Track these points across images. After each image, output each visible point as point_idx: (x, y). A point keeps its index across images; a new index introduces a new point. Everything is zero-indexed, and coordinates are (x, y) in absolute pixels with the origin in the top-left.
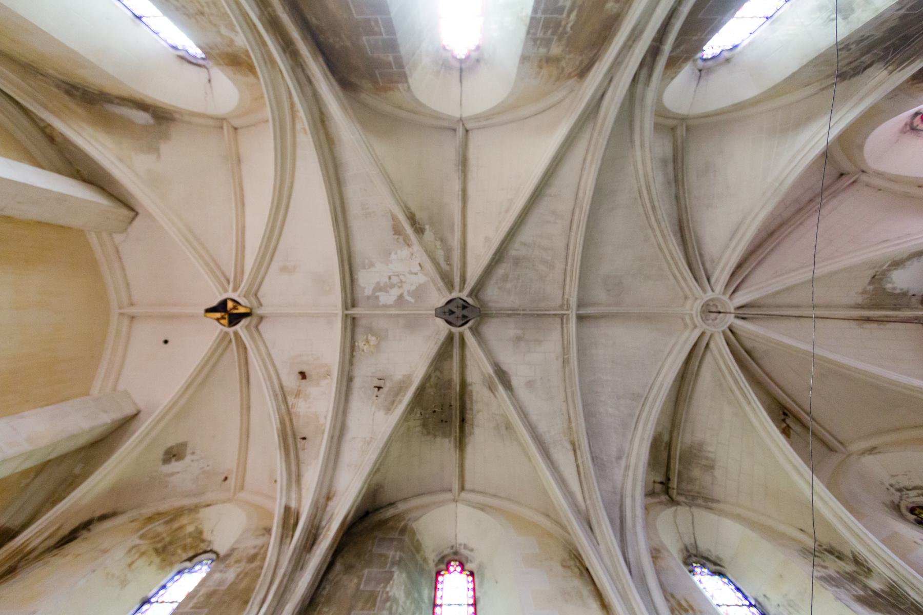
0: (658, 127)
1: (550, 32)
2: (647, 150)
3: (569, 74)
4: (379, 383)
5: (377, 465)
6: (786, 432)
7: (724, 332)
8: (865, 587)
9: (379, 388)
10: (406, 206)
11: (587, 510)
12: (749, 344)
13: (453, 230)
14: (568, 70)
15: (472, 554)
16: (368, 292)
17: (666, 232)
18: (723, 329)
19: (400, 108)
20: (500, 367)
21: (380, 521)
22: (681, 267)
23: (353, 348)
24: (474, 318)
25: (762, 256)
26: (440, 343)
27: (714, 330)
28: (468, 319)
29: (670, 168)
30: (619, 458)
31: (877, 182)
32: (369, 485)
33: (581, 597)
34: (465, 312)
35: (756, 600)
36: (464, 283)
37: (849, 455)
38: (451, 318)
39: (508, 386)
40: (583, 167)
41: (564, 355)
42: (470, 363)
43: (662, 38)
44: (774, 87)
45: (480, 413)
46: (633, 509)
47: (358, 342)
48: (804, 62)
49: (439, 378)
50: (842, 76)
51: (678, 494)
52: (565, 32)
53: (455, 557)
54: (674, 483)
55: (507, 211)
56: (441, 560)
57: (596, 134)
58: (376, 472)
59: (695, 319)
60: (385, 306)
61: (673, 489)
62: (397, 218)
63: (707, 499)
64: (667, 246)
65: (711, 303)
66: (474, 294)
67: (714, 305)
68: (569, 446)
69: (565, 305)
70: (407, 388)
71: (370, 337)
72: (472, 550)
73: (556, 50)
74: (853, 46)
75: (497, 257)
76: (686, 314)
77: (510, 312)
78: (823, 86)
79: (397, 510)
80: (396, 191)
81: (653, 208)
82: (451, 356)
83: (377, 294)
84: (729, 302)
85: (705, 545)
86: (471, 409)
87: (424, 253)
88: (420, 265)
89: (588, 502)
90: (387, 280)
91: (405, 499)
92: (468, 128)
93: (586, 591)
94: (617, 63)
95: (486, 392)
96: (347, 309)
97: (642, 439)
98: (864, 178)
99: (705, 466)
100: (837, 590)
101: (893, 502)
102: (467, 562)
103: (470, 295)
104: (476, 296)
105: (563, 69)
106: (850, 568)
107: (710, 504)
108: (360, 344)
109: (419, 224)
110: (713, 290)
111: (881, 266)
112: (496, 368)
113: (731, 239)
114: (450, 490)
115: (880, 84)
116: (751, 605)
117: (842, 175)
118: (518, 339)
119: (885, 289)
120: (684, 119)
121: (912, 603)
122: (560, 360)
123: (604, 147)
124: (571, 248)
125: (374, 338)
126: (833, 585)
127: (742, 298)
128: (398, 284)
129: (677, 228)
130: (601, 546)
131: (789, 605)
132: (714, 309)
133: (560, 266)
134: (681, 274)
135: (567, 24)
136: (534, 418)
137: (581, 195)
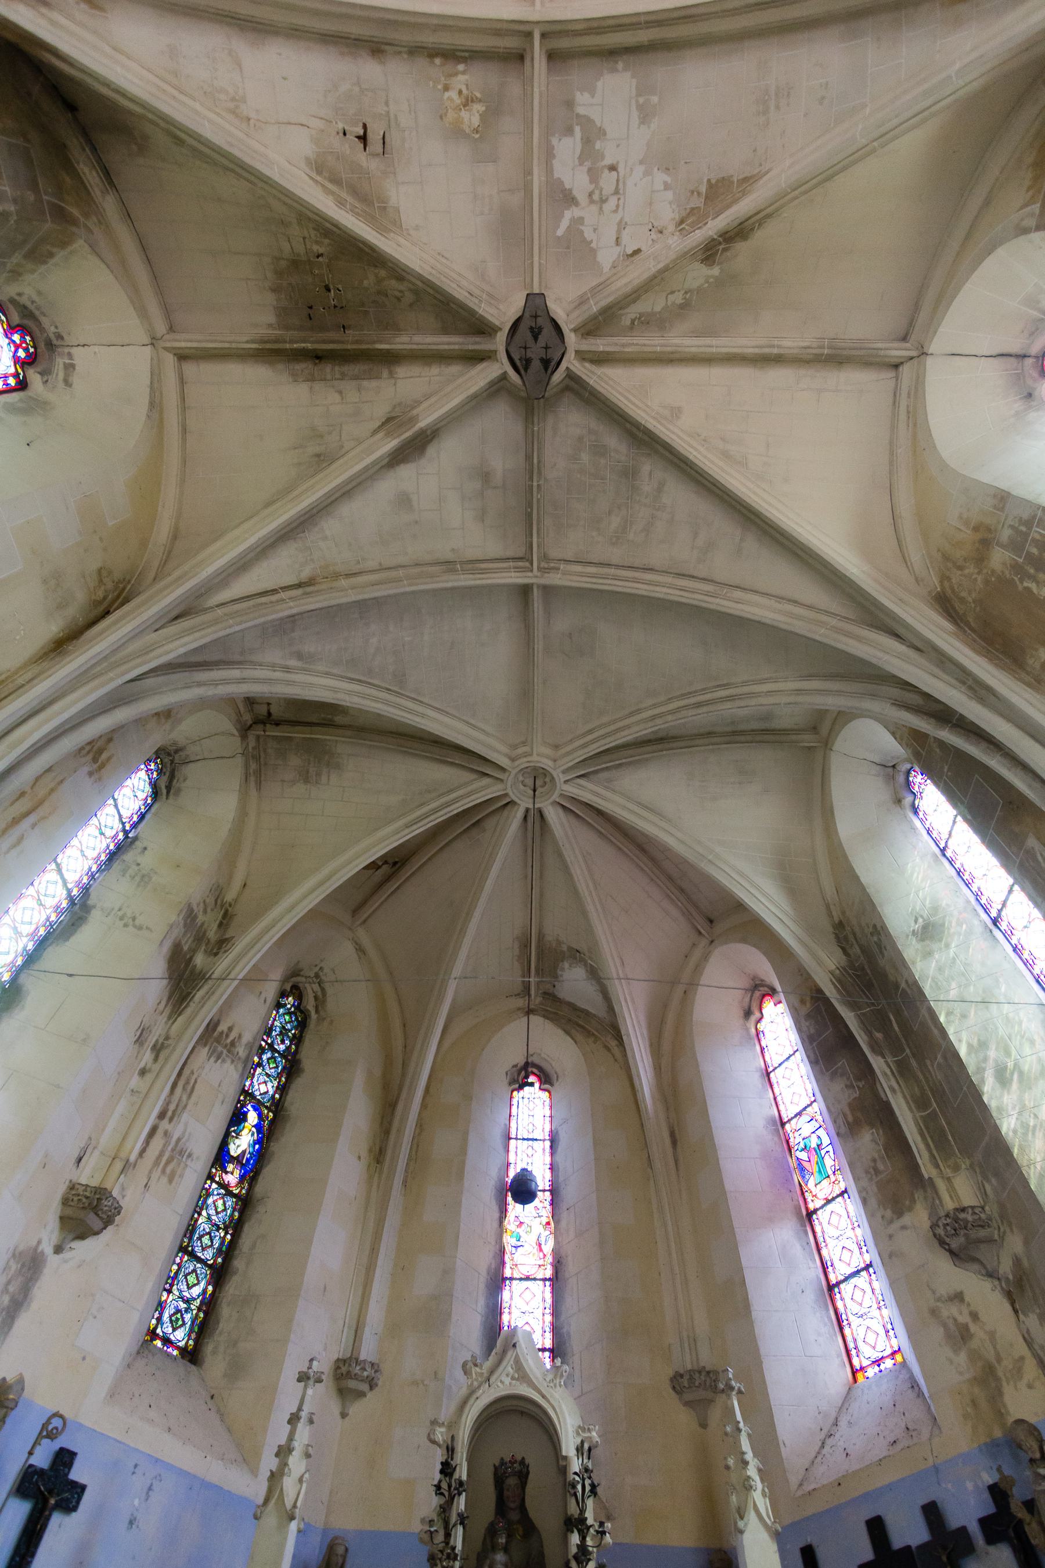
0: (821, 714)
1: (1035, 551)
2: (792, 699)
3: (949, 579)
4: (374, 137)
5: (190, 141)
6: (373, 866)
7: (506, 795)
8: (194, 951)
9: (363, 139)
10: (769, 216)
11: (206, 610)
12: (490, 824)
13: (697, 334)
14: (956, 577)
15: (61, 384)
16: (585, 104)
17: (658, 721)
18: (511, 794)
19: (987, 202)
20: (431, 440)
21: (65, 146)
22: (603, 742)
23: (451, 55)
24: (524, 384)
25: (612, 839)
26: (472, 303)
27: (509, 783)
28: (522, 372)
29: (755, 725)
30: (300, 656)
31: (697, 954)
32: (141, 117)
33: (60, 606)
34: (536, 364)
35: (136, 839)
36: (592, 362)
37: (350, 929)
38: (523, 329)
39: (399, 457)
40: (783, 598)
41: (462, 563)
42: (435, 372)
43: (962, 728)
44: (845, 857)
45: (337, 396)
46: (226, 682)
47: (464, 73)
48: (871, 891)
49: (399, 299)
50: (839, 927)
51: (258, 737)
52: (1025, 576)
53: (42, 346)
54: (273, 732)
55: (726, 455)
56: (26, 312)
57: (834, 622)
58: (176, 137)
59: (525, 760)
60: (549, 154)
61: (264, 731)
62: (744, 193)
63: (258, 774)
64: (638, 723)
65: (547, 780)
66: (572, 384)
67: (545, 783)
68: (305, 575)
69: (549, 564)
70: (371, 219)
71: (479, 107)
72: (67, 383)
73: (999, 558)
74: (875, 939)
75: (640, 435)
76: (532, 749)
77: (535, 461)
78: (832, 907)
79: (98, 193)
80: (806, 192)
81: (699, 705)
82: (445, 331)
83: (577, 129)
84: (551, 800)
85: (192, 775)
86: (343, 377)
87: (661, 266)
88: (637, 252)
89: (220, 612)
90: (608, 161)
91: (128, 215)
92: (901, 369)
93: (74, 611)
94: (942, 660)
95: (381, 410)
96: (543, 35)
97: (335, 690)
98: (704, 942)
99: (308, 772)
100: (182, 925)
101: (301, 970)
102: (41, 374)
103: (570, 375)
104: (567, 388)
105: (960, 568)
106: (212, 934)
107: (252, 779)
108: (461, 78)
109: (725, 250)
110: (566, 782)
111: (590, 958)
112: (429, 432)
113: (640, 804)
114: (171, 329)
115: (820, 963)
116: (126, 833)
117: (711, 921)
118: (486, 477)
119: (562, 961)
120: (827, 744)
121: (190, 993)
122: (450, 556)
123: (809, 635)
124: (649, 576)
125: (476, 121)
126: (185, 921)
127: (554, 816)
128: (597, 192)
129: (660, 735)
130: (154, 635)
131: (143, 876)
132: (539, 783)
133: (615, 554)
134: (593, 742)
135: (1038, 583)
136: (347, 509)
137: (738, 594)
